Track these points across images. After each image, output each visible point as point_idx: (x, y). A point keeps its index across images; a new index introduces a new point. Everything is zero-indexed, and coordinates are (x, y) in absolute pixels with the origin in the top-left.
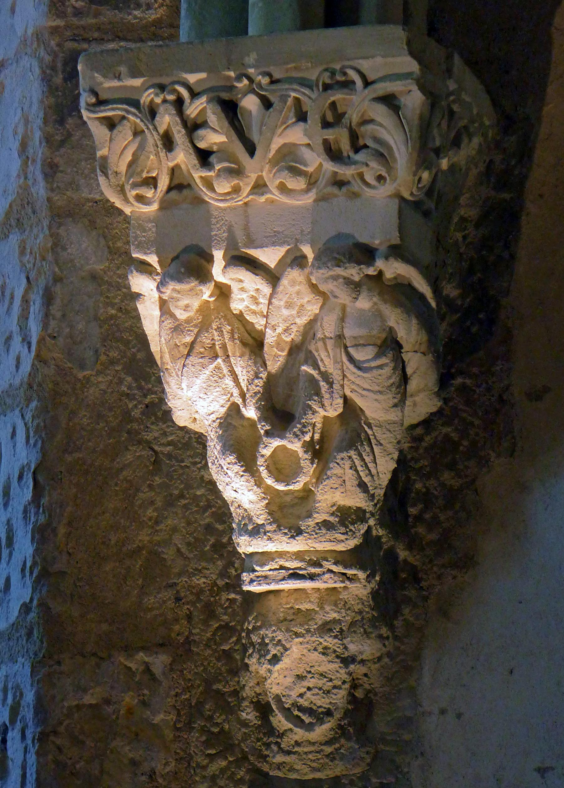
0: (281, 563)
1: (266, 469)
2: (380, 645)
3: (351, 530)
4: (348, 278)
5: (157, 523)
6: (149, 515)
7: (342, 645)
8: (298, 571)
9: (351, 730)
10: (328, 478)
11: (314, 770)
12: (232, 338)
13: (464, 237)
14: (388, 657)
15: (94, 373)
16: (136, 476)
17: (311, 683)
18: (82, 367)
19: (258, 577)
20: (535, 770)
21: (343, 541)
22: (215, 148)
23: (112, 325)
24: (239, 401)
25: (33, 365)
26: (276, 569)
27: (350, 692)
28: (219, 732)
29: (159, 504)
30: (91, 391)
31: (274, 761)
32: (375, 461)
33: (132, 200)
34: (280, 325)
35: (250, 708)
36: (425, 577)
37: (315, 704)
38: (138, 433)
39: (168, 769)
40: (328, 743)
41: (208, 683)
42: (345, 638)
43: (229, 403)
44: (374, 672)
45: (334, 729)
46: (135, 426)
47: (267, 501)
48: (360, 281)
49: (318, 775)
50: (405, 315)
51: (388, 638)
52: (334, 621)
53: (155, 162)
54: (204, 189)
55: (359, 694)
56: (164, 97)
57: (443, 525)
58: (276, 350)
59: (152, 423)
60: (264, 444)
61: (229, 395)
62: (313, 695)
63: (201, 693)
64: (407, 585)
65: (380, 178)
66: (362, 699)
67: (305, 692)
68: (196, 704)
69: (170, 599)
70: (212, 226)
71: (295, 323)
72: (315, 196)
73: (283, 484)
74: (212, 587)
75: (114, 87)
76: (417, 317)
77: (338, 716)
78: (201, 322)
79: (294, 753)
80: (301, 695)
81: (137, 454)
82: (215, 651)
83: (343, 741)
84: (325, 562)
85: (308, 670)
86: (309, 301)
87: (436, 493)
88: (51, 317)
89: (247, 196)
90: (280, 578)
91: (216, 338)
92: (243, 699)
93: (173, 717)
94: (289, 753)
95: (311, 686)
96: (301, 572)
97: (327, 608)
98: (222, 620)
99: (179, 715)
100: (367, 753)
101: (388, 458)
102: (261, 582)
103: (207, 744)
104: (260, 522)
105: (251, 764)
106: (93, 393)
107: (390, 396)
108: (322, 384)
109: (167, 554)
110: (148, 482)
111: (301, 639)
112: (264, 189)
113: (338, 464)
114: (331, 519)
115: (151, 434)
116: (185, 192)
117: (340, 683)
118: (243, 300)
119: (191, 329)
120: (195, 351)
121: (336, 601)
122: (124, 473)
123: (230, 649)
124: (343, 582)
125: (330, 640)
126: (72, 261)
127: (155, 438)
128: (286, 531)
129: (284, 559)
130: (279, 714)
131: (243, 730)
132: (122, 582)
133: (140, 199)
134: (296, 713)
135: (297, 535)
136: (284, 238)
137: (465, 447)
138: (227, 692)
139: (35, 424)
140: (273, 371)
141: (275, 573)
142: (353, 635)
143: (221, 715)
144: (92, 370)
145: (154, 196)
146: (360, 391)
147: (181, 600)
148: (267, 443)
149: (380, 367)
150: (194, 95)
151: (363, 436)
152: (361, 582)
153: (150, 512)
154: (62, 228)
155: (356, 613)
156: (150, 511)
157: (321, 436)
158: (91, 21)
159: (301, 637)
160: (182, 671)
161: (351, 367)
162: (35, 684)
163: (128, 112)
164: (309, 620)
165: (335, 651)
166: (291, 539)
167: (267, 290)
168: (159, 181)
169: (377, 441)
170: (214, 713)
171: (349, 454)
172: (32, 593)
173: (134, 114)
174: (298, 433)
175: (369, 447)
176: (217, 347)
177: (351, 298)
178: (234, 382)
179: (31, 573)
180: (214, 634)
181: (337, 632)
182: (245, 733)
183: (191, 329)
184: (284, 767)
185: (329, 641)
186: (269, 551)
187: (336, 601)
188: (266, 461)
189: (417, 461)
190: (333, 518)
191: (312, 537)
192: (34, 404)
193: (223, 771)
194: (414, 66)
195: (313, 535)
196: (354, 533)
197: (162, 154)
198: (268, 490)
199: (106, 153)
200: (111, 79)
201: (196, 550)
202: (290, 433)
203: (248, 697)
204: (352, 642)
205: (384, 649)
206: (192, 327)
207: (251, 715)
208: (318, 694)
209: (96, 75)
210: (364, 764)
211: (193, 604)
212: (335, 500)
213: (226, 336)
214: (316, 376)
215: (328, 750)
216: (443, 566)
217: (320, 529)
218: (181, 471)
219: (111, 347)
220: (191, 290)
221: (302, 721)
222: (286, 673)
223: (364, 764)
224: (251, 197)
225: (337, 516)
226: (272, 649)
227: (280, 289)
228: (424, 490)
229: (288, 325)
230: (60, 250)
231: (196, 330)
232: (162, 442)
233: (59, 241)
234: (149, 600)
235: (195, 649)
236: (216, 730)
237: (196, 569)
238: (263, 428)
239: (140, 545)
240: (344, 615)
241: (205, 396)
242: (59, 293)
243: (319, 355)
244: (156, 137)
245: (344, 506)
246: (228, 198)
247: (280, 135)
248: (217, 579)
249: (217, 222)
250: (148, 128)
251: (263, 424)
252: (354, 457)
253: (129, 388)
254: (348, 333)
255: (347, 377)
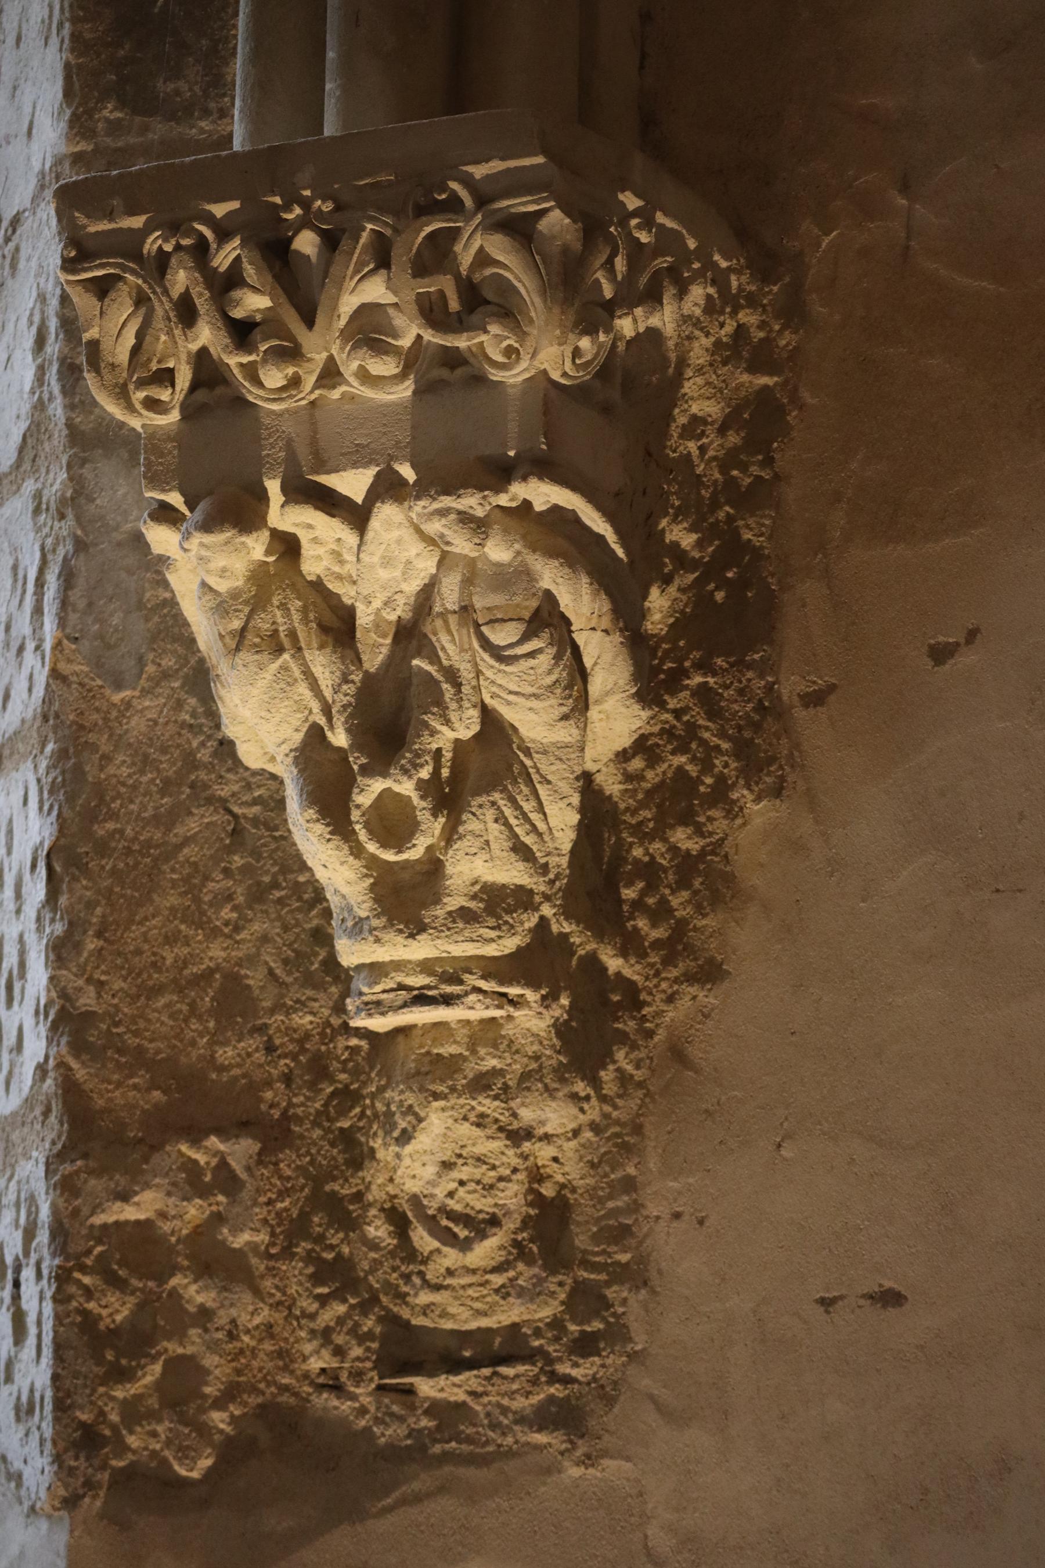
0: (399, 979)
1: (364, 827)
2: (574, 1111)
3: (506, 922)
4: (465, 513)
5: (237, 929)
6: (226, 917)
7: (508, 1110)
8: (426, 992)
9: (535, 1249)
10: (460, 838)
11: (479, 1313)
12: (305, 620)
13: (702, 449)
14: (592, 1130)
15: (137, 693)
16: (204, 855)
17: (464, 1172)
18: (119, 686)
19: (367, 1004)
20: (816, 1301)
21: (492, 940)
22: (258, 317)
23: (165, 616)
24: (322, 721)
25: (48, 685)
26: (392, 990)
27: (531, 1190)
28: (334, 1259)
29: (241, 899)
30: (133, 723)
31: (417, 1301)
32: (541, 809)
33: (138, 406)
34: (378, 595)
35: (380, 1219)
36: (649, 999)
37: (472, 1208)
38: (206, 786)
39: (257, 1320)
40: (497, 1269)
41: (318, 1181)
42: (512, 1099)
43: (307, 725)
44: (570, 1154)
45: (505, 1248)
46: (203, 775)
47: (372, 880)
48: (485, 516)
49: (484, 1323)
50: (567, 570)
51: (587, 1098)
52: (495, 1072)
53: (170, 344)
54: (246, 384)
55: (548, 1191)
56: (177, 241)
57: (676, 913)
58: (373, 635)
59: (229, 770)
60: (358, 787)
61: (307, 712)
62: (469, 1192)
63: (307, 1198)
64: (620, 1014)
65: (509, 351)
66: (553, 1199)
67: (456, 1189)
68: (299, 1215)
69: (257, 1050)
70: (263, 442)
71: (401, 592)
72: (413, 387)
73: (393, 851)
74: (324, 1029)
75: (103, 231)
76: (589, 574)
77: (512, 1226)
78: (254, 596)
79: (447, 1287)
80: (451, 1194)
81: (206, 820)
82: (328, 1131)
83: (521, 1266)
84: (468, 976)
85: (458, 1151)
86: (418, 555)
87: (664, 862)
88: (70, 608)
89: (312, 392)
90: (399, 1003)
91: (280, 620)
92: (370, 1205)
93: (262, 1237)
94: (438, 1288)
95: (465, 1178)
96: (430, 993)
97: (482, 1051)
98: (340, 1082)
99: (273, 1234)
100: (561, 1284)
101: (562, 804)
102: (372, 1011)
103: (317, 1279)
104: (363, 914)
105: (384, 1308)
106: (136, 725)
107: (554, 702)
108: (445, 686)
109: (253, 978)
110: (223, 865)
111: (442, 1103)
112: (338, 379)
113: (474, 814)
114: (472, 905)
115: (227, 788)
116: (219, 391)
117: (508, 1172)
118: (319, 558)
119: (240, 607)
120: (246, 642)
121: (495, 1040)
122: (186, 851)
123: (351, 1126)
124: (500, 1007)
125: (487, 1102)
126: (102, 518)
127: (233, 795)
128: (401, 927)
129: (403, 972)
130: (418, 1225)
131: (373, 1255)
132: (183, 1026)
133: (153, 405)
134: (445, 1222)
135: (418, 933)
136: (370, 454)
137: (708, 786)
138: (347, 1195)
139: (50, 780)
140: (372, 670)
141: (392, 995)
142: (526, 1093)
143: (337, 1232)
144: (134, 689)
145: (172, 400)
146: (506, 696)
147: (275, 1051)
148: (364, 785)
149: (531, 655)
150: (224, 234)
151: (516, 768)
152: (530, 1008)
153: (227, 913)
154: (86, 466)
155: (530, 1058)
156: (227, 910)
157: (451, 772)
158: (133, 140)
159: (443, 1099)
160: (276, 1164)
161: (486, 656)
162: (51, 1191)
163: (125, 268)
164: (455, 1072)
165: (496, 1121)
166: (410, 940)
167: (351, 538)
168: (177, 375)
169: (542, 776)
170: (327, 1230)
171: (491, 798)
172: (47, 1048)
173: (133, 272)
174: (408, 766)
175: (527, 786)
176: (282, 635)
177: (471, 545)
178: (312, 690)
179: (46, 1016)
180: (326, 1105)
181: (499, 1089)
182: (375, 1260)
183: (240, 607)
184: (432, 1311)
185: (487, 1105)
186: (381, 960)
187: (495, 1040)
188: (363, 815)
189: (634, 812)
190: (474, 903)
191: (443, 934)
192: (50, 747)
193: (340, 1321)
195: (443, 931)
196: (512, 927)
197: (177, 332)
198: (373, 862)
199: (97, 336)
200: (100, 219)
201: (298, 971)
202: (396, 769)
203: (376, 1201)
204: (523, 1104)
205: (581, 1116)
206: (241, 604)
207: (382, 1230)
208: (475, 1191)
209: (77, 214)
210: (556, 1303)
211: (295, 1057)
212: (476, 873)
213: (295, 617)
214: (435, 674)
215: (498, 1280)
216: (676, 980)
217: (454, 922)
218: (273, 846)
219: (164, 651)
220: (226, 543)
221: (455, 1236)
222: (425, 1158)
223: (556, 1303)
224: (317, 392)
225: (482, 900)
226: (400, 1121)
227: (370, 535)
228: (647, 859)
229: (390, 594)
230: (83, 501)
231: (247, 610)
232: (244, 799)
233: (83, 487)
234: (225, 1052)
235: (297, 1129)
236: (329, 1256)
237: (298, 1001)
238: (358, 762)
239: (211, 964)
240: (509, 1061)
241: (269, 716)
242: (83, 569)
243: (438, 640)
244: (168, 306)
245: (493, 884)
246: (285, 395)
247: (353, 291)
248: (330, 1016)
249: (269, 435)
250: (155, 292)
251: (356, 755)
252: (501, 803)
253: (194, 714)
254: (479, 602)
255: (483, 674)
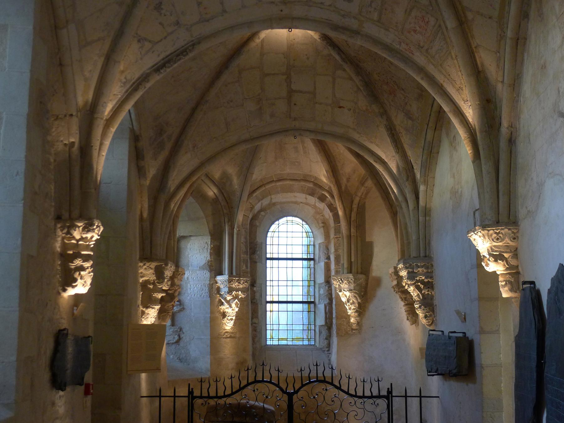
194: (353, 277)
